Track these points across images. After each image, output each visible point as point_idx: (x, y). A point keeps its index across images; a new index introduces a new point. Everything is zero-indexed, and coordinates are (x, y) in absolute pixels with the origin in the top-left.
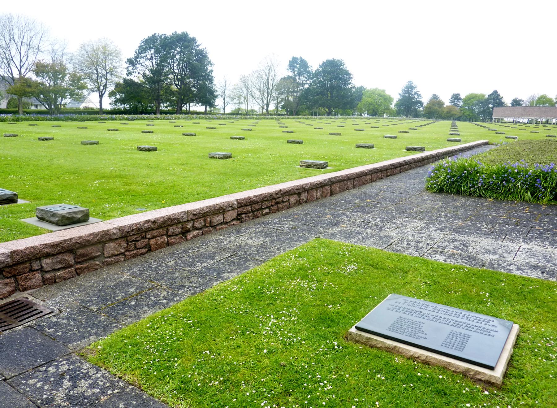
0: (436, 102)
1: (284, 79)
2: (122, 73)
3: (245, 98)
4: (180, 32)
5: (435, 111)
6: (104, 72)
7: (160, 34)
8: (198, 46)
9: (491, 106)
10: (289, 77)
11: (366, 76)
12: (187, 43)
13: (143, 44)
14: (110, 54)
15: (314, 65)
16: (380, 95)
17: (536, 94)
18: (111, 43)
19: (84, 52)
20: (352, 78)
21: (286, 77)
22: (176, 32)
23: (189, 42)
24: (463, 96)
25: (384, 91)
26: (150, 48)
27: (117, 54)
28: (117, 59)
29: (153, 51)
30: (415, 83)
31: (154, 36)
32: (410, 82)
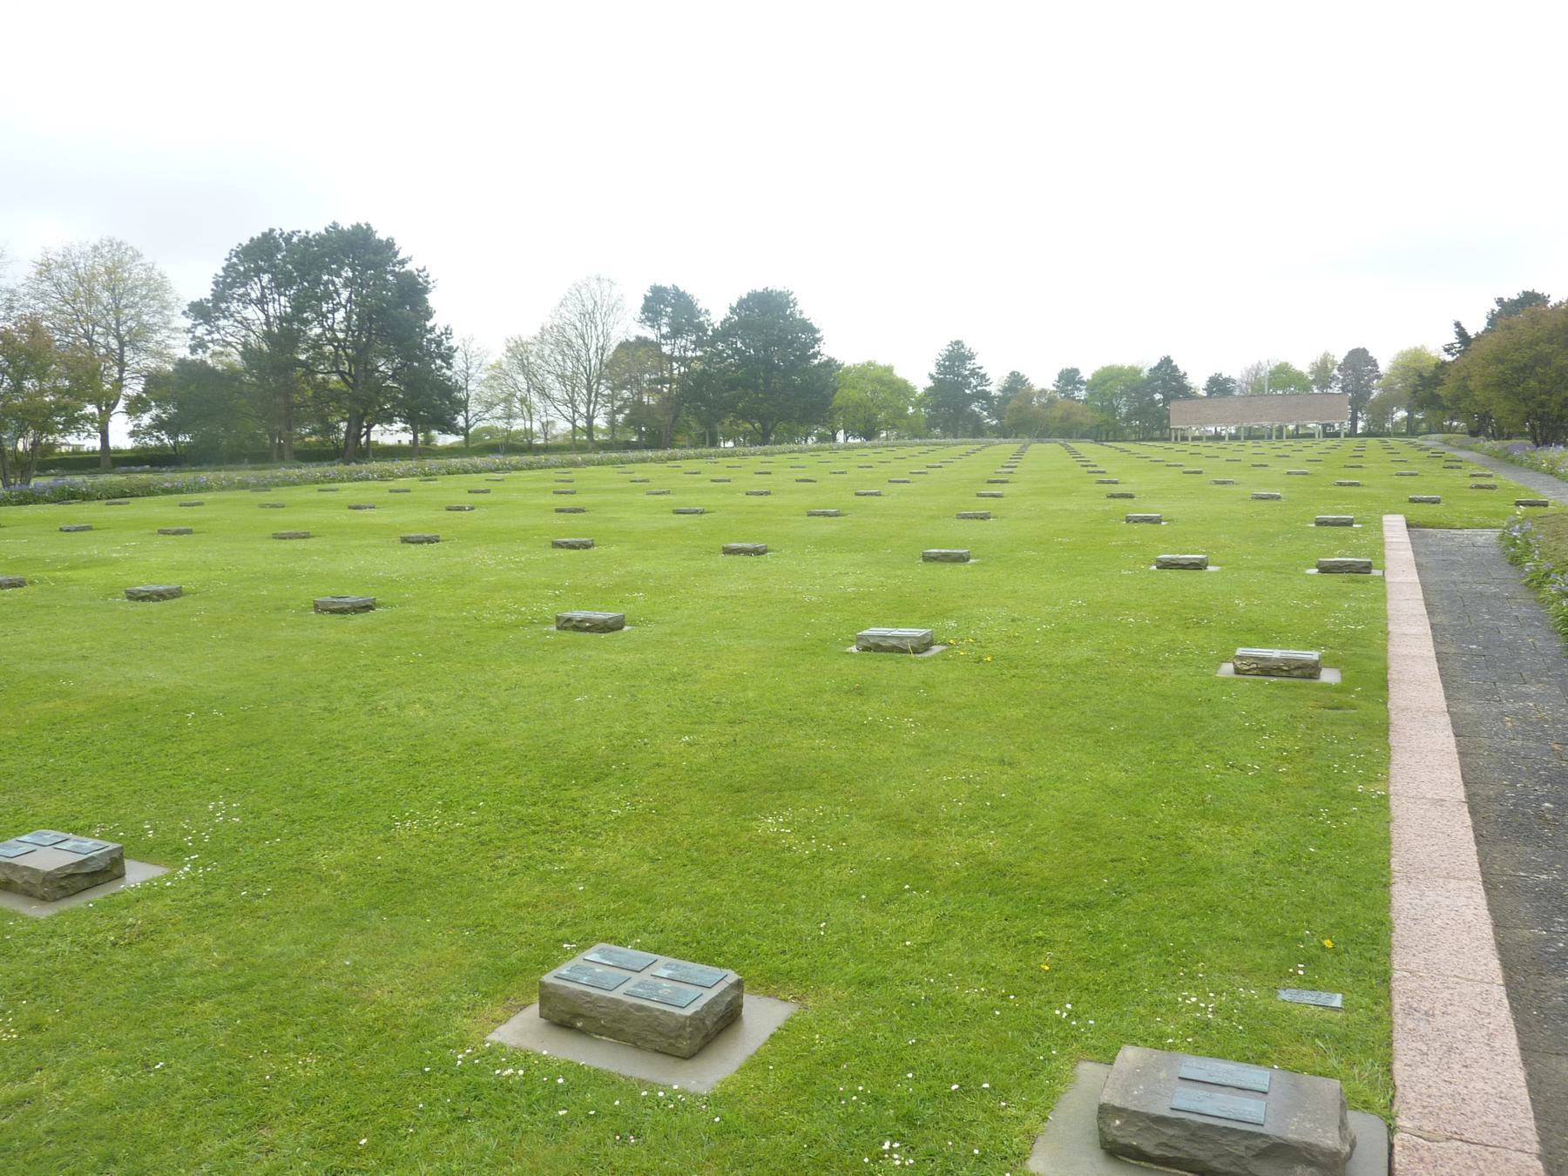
0: (886, 384)
1: (624, 346)
2: (177, 343)
3: (523, 401)
4: (346, 224)
5: (1022, 416)
6: (114, 344)
7: (287, 231)
8: (403, 262)
9: (1158, 396)
10: (642, 342)
11: (857, 333)
12: (372, 257)
13: (235, 260)
14: (132, 291)
15: (716, 309)
16: (880, 381)
17: (1264, 363)
18: (133, 259)
19: (47, 286)
20: (819, 340)
21: (632, 340)
22: (335, 226)
23: (376, 253)
24: (1086, 375)
25: (889, 369)
26: (259, 271)
27: (156, 289)
28: (155, 304)
29: (266, 278)
30: (970, 345)
31: (268, 237)
32: (957, 343)
